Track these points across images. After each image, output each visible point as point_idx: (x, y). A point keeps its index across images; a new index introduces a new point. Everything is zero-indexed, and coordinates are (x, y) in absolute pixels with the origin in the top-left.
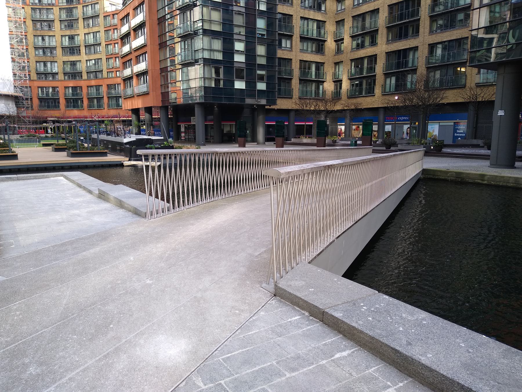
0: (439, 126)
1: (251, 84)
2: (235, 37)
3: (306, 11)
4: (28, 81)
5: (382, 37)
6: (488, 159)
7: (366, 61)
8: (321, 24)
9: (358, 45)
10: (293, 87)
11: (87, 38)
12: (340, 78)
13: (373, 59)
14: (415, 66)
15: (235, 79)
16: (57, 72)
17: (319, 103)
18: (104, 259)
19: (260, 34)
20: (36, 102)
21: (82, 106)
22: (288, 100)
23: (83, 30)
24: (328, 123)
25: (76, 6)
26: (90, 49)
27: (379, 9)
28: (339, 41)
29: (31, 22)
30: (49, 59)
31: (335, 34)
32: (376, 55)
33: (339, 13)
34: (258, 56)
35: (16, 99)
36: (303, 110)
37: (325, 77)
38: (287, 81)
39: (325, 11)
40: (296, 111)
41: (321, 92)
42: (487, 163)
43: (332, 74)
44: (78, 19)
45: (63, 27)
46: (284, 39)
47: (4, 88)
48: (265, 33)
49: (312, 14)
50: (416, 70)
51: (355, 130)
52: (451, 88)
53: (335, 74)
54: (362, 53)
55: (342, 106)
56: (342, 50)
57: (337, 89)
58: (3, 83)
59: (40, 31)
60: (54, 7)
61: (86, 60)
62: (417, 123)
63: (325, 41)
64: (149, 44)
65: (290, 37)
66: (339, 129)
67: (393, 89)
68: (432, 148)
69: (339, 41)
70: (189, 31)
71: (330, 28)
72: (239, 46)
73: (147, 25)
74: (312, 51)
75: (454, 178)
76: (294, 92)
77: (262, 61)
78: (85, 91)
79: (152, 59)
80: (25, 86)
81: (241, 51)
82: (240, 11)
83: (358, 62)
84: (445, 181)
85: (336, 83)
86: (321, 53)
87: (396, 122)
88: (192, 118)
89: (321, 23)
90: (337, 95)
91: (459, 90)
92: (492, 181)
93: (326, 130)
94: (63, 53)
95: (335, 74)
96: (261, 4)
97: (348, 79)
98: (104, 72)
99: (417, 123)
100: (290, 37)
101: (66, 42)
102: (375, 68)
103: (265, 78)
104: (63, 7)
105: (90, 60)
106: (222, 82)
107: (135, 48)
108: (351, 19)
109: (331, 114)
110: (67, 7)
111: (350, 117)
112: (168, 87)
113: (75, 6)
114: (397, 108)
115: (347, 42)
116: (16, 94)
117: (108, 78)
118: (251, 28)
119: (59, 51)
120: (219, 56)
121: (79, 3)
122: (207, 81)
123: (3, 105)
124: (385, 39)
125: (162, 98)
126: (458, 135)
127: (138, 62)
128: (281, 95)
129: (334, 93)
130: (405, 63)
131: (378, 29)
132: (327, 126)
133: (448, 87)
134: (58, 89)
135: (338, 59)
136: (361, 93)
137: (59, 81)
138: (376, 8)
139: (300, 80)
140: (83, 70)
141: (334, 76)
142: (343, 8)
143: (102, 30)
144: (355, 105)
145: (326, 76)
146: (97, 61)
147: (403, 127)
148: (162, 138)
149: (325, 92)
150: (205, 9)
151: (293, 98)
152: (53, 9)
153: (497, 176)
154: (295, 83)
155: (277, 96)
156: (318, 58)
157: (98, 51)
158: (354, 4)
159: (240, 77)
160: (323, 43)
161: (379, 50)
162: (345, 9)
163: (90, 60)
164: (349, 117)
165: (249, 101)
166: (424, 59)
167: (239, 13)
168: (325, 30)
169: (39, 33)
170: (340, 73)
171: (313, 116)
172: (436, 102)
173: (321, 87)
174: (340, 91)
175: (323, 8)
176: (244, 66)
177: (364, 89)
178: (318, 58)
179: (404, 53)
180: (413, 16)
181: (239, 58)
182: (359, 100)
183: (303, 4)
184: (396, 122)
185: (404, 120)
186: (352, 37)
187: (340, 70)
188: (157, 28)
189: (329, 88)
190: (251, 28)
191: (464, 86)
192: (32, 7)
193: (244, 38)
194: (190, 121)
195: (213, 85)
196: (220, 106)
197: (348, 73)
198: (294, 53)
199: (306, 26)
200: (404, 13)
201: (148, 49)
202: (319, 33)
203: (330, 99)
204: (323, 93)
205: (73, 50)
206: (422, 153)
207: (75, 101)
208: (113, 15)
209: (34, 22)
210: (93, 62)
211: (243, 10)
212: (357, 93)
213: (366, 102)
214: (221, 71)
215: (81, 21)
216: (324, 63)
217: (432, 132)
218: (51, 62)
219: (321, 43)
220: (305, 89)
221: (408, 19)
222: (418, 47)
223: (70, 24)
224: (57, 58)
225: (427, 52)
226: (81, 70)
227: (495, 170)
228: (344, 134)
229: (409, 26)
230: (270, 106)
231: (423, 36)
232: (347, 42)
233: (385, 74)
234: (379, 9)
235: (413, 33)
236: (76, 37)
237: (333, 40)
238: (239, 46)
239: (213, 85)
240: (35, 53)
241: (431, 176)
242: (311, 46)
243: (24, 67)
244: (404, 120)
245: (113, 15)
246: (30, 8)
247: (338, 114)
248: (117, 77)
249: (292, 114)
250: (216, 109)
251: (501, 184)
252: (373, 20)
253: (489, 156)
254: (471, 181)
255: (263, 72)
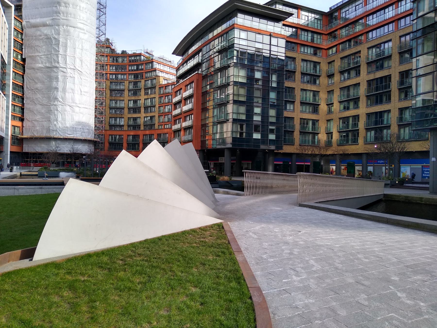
0: (411, 168)
1: (264, 136)
2: (255, 104)
3: (305, 85)
4: (104, 131)
5: (363, 102)
6: (428, 190)
7: (351, 119)
8: (315, 93)
9: (344, 108)
10: (294, 137)
11: (146, 102)
12: (331, 131)
13: (356, 118)
14: (389, 124)
15: (253, 132)
16: (123, 124)
17: (315, 149)
18: (113, 284)
19: (272, 102)
20: (107, 145)
21: (138, 149)
22: (292, 146)
23: (143, 96)
24: (322, 164)
25: (140, 80)
26: (148, 109)
27: (360, 83)
28: (330, 105)
29: (109, 91)
30: (118, 116)
31: (327, 100)
32: (359, 115)
33: (330, 86)
34: (270, 116)
35: (94, 143)
36: (303, 154)
37: (319, 130)
38: (290, 133)
39: (319, 84)
40: (297, 154)
41: (316, 141)
42: (428, 192)
43: (324, 128)
44: (141, 89)
45: (130, 94)
46: (288, 104)
47: (88, 136)
48: (275, 101)
49: (309, 87)
50: (390, 126)
51: (344, 170)
52: (417, 140)
53: (327, 128)
54: (347, 114)
55: (333, 151)
56: (332, 111)
57: (329, 139)
58: (89, 132)
59: (115, 97)
60: (125, 81)
61: (144, 117)
62: (393, 166)
63: (319, 105)
64: (195, 108)
65: (293, 102)
66: (331, 169)
67: (373, 139)
68: (397, 182)
69: (330, 105)
70: (223, 101)
71: (323, 96)
72: (257, 110)
73: (195, 96)
74: (309, 112)
75: (404, 200)
76: (296, 141)
77: (273, 120)
78: (141, 138)
79: (196, 118)
80: (101, 134)
81: (259, 114)
82: (259, 88)
83: (345, 120)
84: (399, 201)
85: (328, 135)
86: (316, 113)
87: (375, 165)
88: (219, 158)
89: (316, 92)
90: (329, 144)
91: (424, 142)
92: (428, 202)
93: (320, 168)
94: (128, 112)
95: (327, 128)
96: (273, 82)
97: (338, 132)
98: (156, 125)
99: (393, 166)
100: (293, 102)
101: (131, 105)
102: (358, 124)
103: (275, 131)
104: (131, 81)
105: (147, 117)
106: (244, 134)
107: (184, 111)
108: (339, 90)
109: (324, 157)
110: (134, 81)
111: (340, 160)
112: (206, 137)
113: (139, 80)
114: (376, 154)
115: (336, 107)
116: (96, 140)
117: (158, 129)
118: (265, 98)
119: (126, 110)
120: (243, 117)
121: (143, 79)
122: (234, 134)
123: (87, 147)
124: (365, 104)
125: (201, 145)
126: (425, 175)
127: (185, 121)
128: (285, 143)
129: (327, 141)
130: (381, 121)
131: (360, 97)
132: (322, 166)
133: (415, 140)
134: (123, 136)
135: (329, 117)
136: (347, 142)
137: (124, 131)
138: (357, 83)
139: (300, 132)
140: (141, 124)
141: (326, 130)
142: (333, 82)
143: (157, 96)
144: (343, 151)
145: (320, 129)
146: (152, 117)
147: (382, 168)
148: (208, 171)
149: (320, 141)
150: (235, 87)
151: (295, 145)
152: (124, 82)
153: (430, 198)
154: (297, 134)
155: (283, 143)
156: (314, 117)
157: (153, 111)
158: (341, 79)
159: (257, 131)
160: (317, 106)
161: (361, 112)
162: (334, 83)
163: (147, 117)
164: (338, 160)
165: (262, 147)
166: (396, 119)
167: (258, 89)
168: (319, 97)
169: (113, 98)
170: (331, 127)
171: (310, 158)
172: (400, 150)
173: (316, 137)
174: (331, 140)
175: (318, 82)
176: (260, 123)
177: (350, 139)
178: (314, 117)
179: (380, 114)
180: (385, 89)
181: (257, 118)
182: (347, 147)
183: (303, 79)
184: (375, 165)
185: (382, 163)
186: (340, 102)
187: (331, 125)
188: (201, 98)
189: (322, 138)
190: (265, 98)
191: (427, 139)
192: (111, 81)
193: (261, 105)
194: (218, 160)
195: (238, 136)
196: (242, 151)
197: (337, 128)
198: (295, 113)
199: (304, 95)
200: (379, 86)
201: (194, 112)
202: (315, 99)
203: (323, 146)
204: (318, 141)
205: (136, 110)
206: (383, 184)
207: (134, 145)
208: (166, 87)
209: (111, 91)
210: (149, 118)
211: (261, 87)
212: (345, 142)
213: (352, 149)
214: (244, 127)
215: (143, 92)
216: (319, 120)
217: (405, 173)
218: (120, 118)
219: (316, 106)
220: (304, 138)
221: (382, 90)
222: (390, 110)
223: (136, 92)
224: (124, 115)
225: (397, 114)
226: (140, 123)
227: (431, 195)
228: (335, 173)
229: (383, 95)
230: (278, 151)
231: (394, 103)
232: (336, 107)
233: (366, 129)
234: (360, 83)
235: (386, 100)
236: (138, 101)
237: (325, 104)
238: (257, 110)
239: (238, 136)
240: (110, 111)
241: (390, 199)
242: (309, 109)
243: (102, 121)
244: (382, 163)
245: (166, 87)
246: (109, 82)
247: (330, 157)
248: (165, 128)
249: (294, 157)
250: (238, 152)
251: (433, 203)
252: (356, 91)
253: (429, 188)
254: (415, 202)
255: (273, 128)
